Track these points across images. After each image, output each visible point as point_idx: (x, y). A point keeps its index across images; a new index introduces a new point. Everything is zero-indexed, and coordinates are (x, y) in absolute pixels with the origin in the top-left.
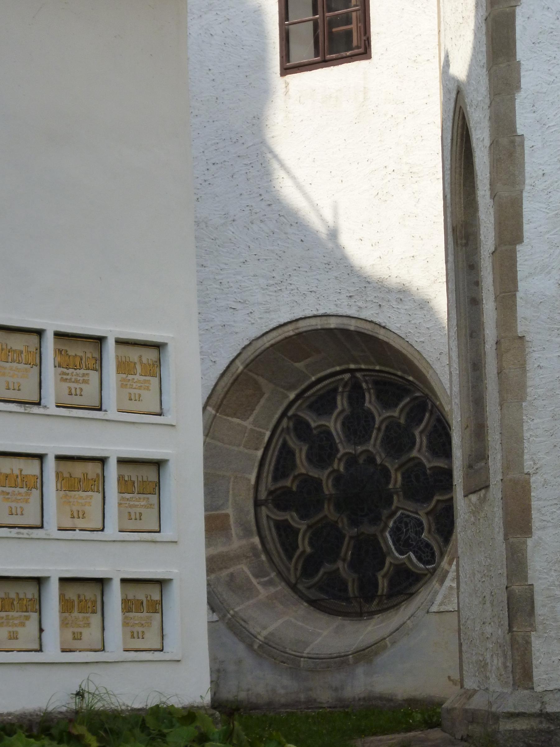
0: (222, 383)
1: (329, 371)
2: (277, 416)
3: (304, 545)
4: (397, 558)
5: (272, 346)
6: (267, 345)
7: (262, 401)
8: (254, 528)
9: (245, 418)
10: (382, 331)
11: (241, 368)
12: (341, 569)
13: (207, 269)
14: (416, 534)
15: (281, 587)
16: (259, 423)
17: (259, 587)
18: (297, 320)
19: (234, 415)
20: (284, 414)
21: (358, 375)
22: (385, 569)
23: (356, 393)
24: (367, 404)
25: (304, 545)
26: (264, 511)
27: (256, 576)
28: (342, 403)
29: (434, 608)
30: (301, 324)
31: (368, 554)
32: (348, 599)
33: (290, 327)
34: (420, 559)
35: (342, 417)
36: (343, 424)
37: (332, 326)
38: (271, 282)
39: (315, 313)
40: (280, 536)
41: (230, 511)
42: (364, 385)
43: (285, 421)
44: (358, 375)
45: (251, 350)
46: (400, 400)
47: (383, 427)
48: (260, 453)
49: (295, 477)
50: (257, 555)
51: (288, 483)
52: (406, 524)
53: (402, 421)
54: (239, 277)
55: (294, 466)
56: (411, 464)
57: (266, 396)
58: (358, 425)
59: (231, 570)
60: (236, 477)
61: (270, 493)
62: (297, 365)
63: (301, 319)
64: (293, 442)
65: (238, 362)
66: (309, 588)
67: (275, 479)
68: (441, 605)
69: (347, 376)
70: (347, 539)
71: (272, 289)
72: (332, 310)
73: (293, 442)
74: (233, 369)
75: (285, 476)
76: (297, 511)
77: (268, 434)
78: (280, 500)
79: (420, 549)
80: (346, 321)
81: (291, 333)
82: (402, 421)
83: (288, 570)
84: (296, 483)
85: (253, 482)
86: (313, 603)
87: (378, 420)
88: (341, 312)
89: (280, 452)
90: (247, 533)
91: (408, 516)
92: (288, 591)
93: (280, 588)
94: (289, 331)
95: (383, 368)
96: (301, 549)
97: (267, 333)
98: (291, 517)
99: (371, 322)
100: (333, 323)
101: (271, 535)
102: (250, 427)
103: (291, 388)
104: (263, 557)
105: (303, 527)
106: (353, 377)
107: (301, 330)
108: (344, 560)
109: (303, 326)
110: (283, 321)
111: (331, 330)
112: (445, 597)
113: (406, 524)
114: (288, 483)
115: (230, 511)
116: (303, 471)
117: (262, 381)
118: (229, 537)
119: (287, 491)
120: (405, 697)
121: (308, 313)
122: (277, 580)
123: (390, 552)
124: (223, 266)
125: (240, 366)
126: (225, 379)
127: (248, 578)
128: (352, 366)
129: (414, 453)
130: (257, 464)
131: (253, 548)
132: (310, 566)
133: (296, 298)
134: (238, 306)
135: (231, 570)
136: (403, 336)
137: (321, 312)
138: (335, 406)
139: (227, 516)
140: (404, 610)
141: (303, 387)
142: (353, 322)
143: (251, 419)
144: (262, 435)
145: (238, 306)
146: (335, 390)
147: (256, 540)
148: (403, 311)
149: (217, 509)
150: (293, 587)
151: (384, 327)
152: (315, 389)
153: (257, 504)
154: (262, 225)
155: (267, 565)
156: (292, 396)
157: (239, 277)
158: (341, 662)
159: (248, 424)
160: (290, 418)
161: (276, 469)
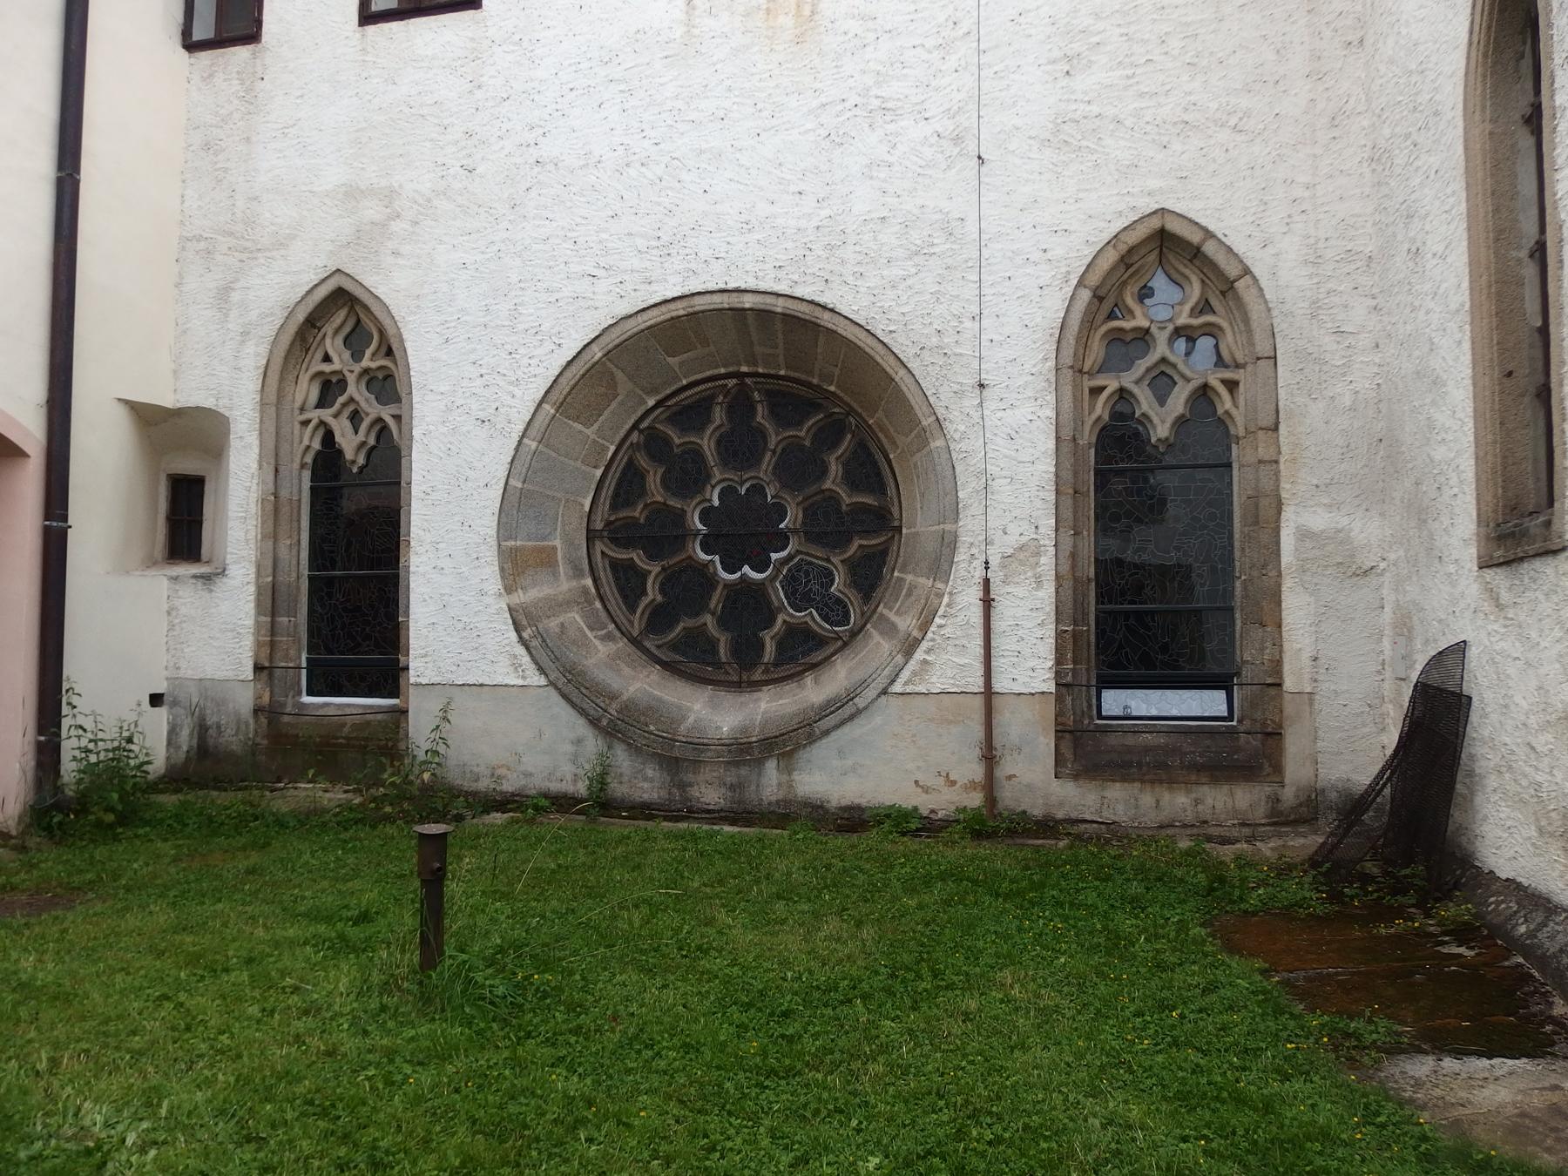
0: (568, 374)
1: (709, 373)
2: (627, 427)
3: (652, 593)
4: (792, 616)
5: (648, 328)
6: (642, 327)
7: (614, 405)
8: (586, 567)
9: (588, 425)
10: (827, 315)
11: (599, 355)
12: (710, 625)
13: (554, 224)
14: (822, 585)
15: (622, 643)
16: (604, 434)
17: (597, 642)
18: (693, 295)
19: (577, 419)
20: (635, 427)
21: (748, 381)
22: (776, 629)
23: (740, 406)
24: (759, 419)
25: (652, 593)
26: (599, 546)
27: (592, 629)
28: (719, 415)
29: (897, 687)
30: (698, 300)
31: (748, 607)
32: (718, 665)
33: (679, 304)
34: (826, 618)
35: (717, 434)
36: (718, 443)
37: (747, 306)
38: (655, 243)
39: (723, 286)
40: (617, 579)
41: (557, 543)
42: (756, 395)
43: (635, 435)
44: (748, 381)
45: (617, 331)
46: (807, 416)
47: (779, 450)
48: (599, 473)
49: (646, 506)
50: (591, 603)
51: (637, 512)
52: (807, 574)
53: (807, 443)
54: (604, 236)
55: (643, 492)
56: (819, 497)
57: (619, 398)
58: (741, 447)
59: (561, 619)
60: (567, 501)
61: (608, 524)
62: (669, 359)
63: (699, 293)
64: (642, 461)
65: (594, 347)
66: (658, 647)
67: (614, 507)
68: (906, 684)
69: (732, 382)
70: (720, 588)
71: (655, 252)
72: (751, 284)
73: (642, 461)
74: (585, 356)
75: (629, 504)
76: (643, 549)
77: (612, 448)
78: (619, 534)
79: (826, 605)
80: (769, 300)
81: (682, 312)
82: (807, 443)
83: (632, 623)
84: (646, 513)
85: (587, 509)
86: (666, 666)
87: (773, 441)
88: (763, 286)
89: (624, 473)
90: (577, 573)
91: (811, 563)
92: (631, 649)
93: (621, 644)
94: (679, 309)
95: (792, 374)
96: (651, 596)
97: (644, 310)
98: (637, 556)
99: (812, 302)
100: (748, 302)
101: (606, 576)
102: (593, 436)
103: (652, 391)
104: (598, 605)
105: (655, 569)
106: (743, 384)
107: (697, 308)
108: (713, 614)
109: (701, 304)
110: (670, 295)
111: (744, 310)
112: (914, 674)
113: (807, 574)
114: (637, 512)
115: (557, 543)
116: (660, 499)
117: (619, 375)
118: (555, 575)
119: (632, 523)
120: (844, 802)
121: (711, 286)
122: (618, 634)
123: (782, 609)
124: (579, 220)
125: (597, 353)
126: (573, 368)
127: (581, 630)
128: (744, 369)
129: (828, 485)
130: (594, 486)
131: (585, 591)
132: (659, 619)
133: (693, 266)
134: (600, 273)
135: (561, 619)
136: (863, 323)
137: (731, 286)
138: (709, 420)
139: (554, 548)
140: (195, 577)
141: (668, 391)
142: (781, 302)
143: (596, 426)
144: (605, 449)
145: (600, 273)
146: (712, 397)
147: (589, 582)
148: (863, 290)
149: (544, 539)
150: (635, 642)
151: (832, 310)
152: (682, 396)
153: (591, 536)
154: (643, 169)
155: (603, 614)
156: (651, 402)
157: (604, 236)
158: (748, 752)
159: (590, 432)
160: (641, 431)
161: (616, 495)
